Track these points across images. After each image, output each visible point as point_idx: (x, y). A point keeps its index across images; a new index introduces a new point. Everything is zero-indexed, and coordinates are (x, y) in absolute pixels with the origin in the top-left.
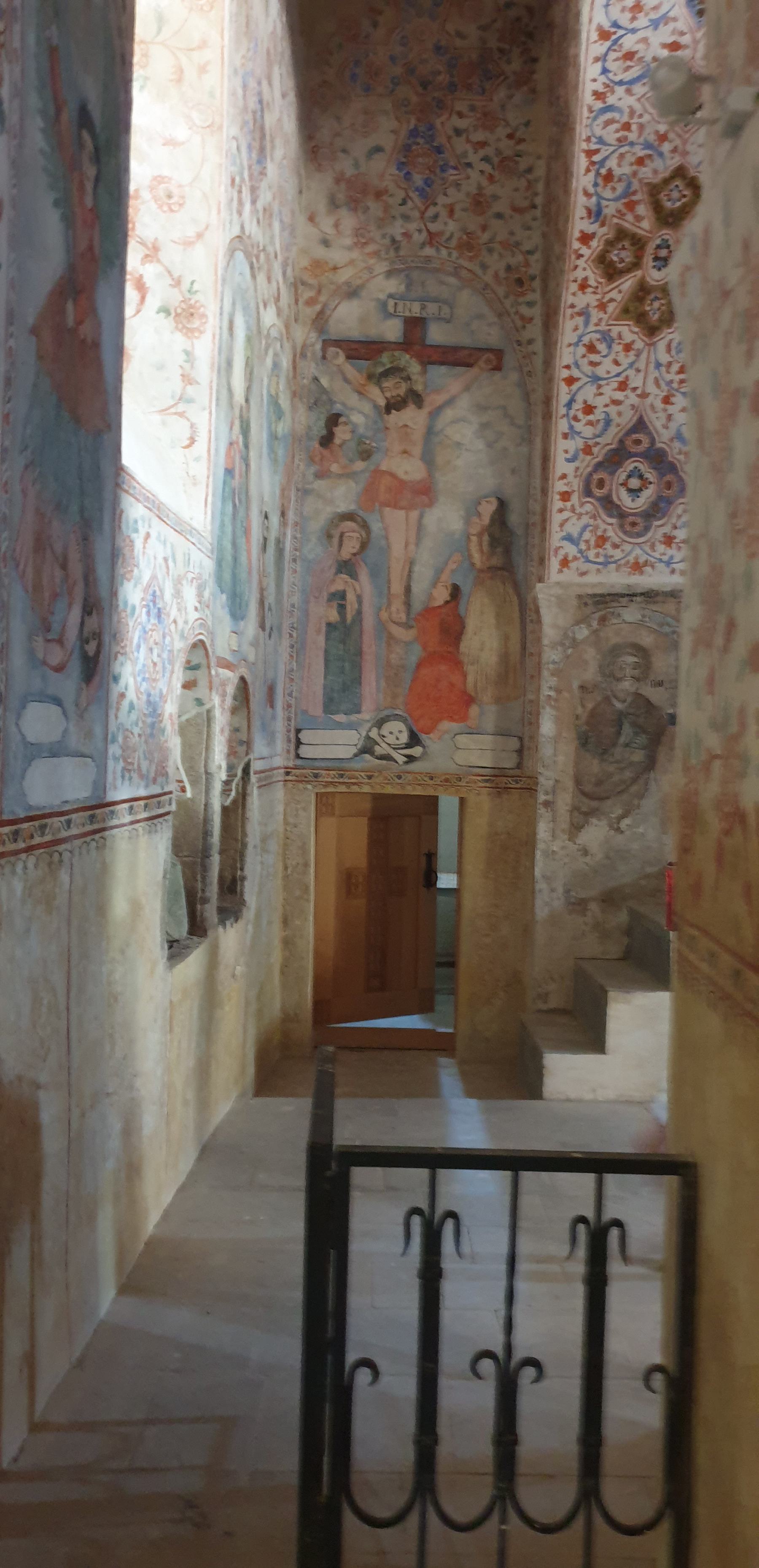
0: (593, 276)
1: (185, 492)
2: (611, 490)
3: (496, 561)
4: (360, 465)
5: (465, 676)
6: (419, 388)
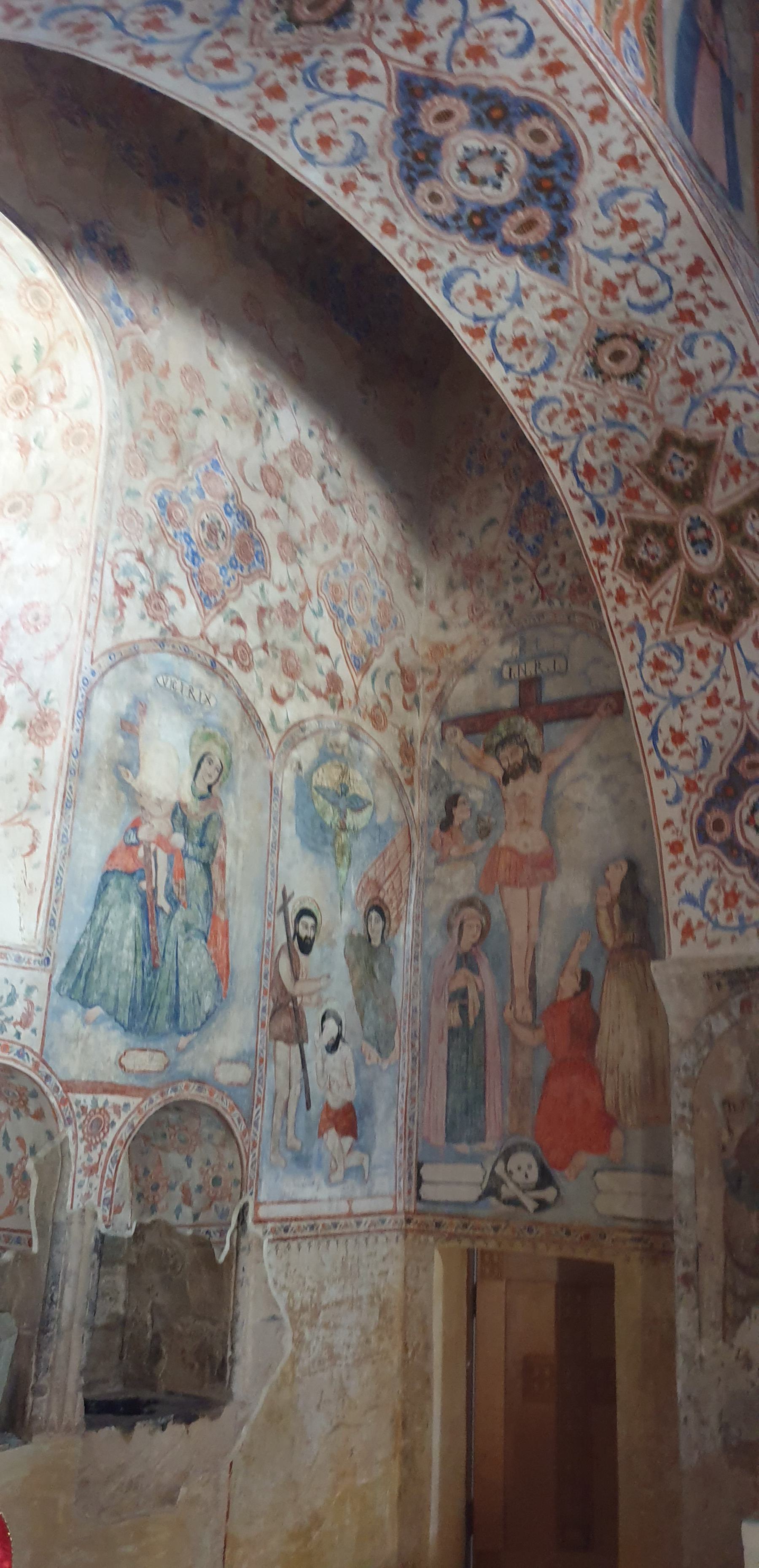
1: (19, 901)
2: (733, 831)
3: (629, 937)
4: (479, 844)
5: (602, 1089)
6: (536, 750)
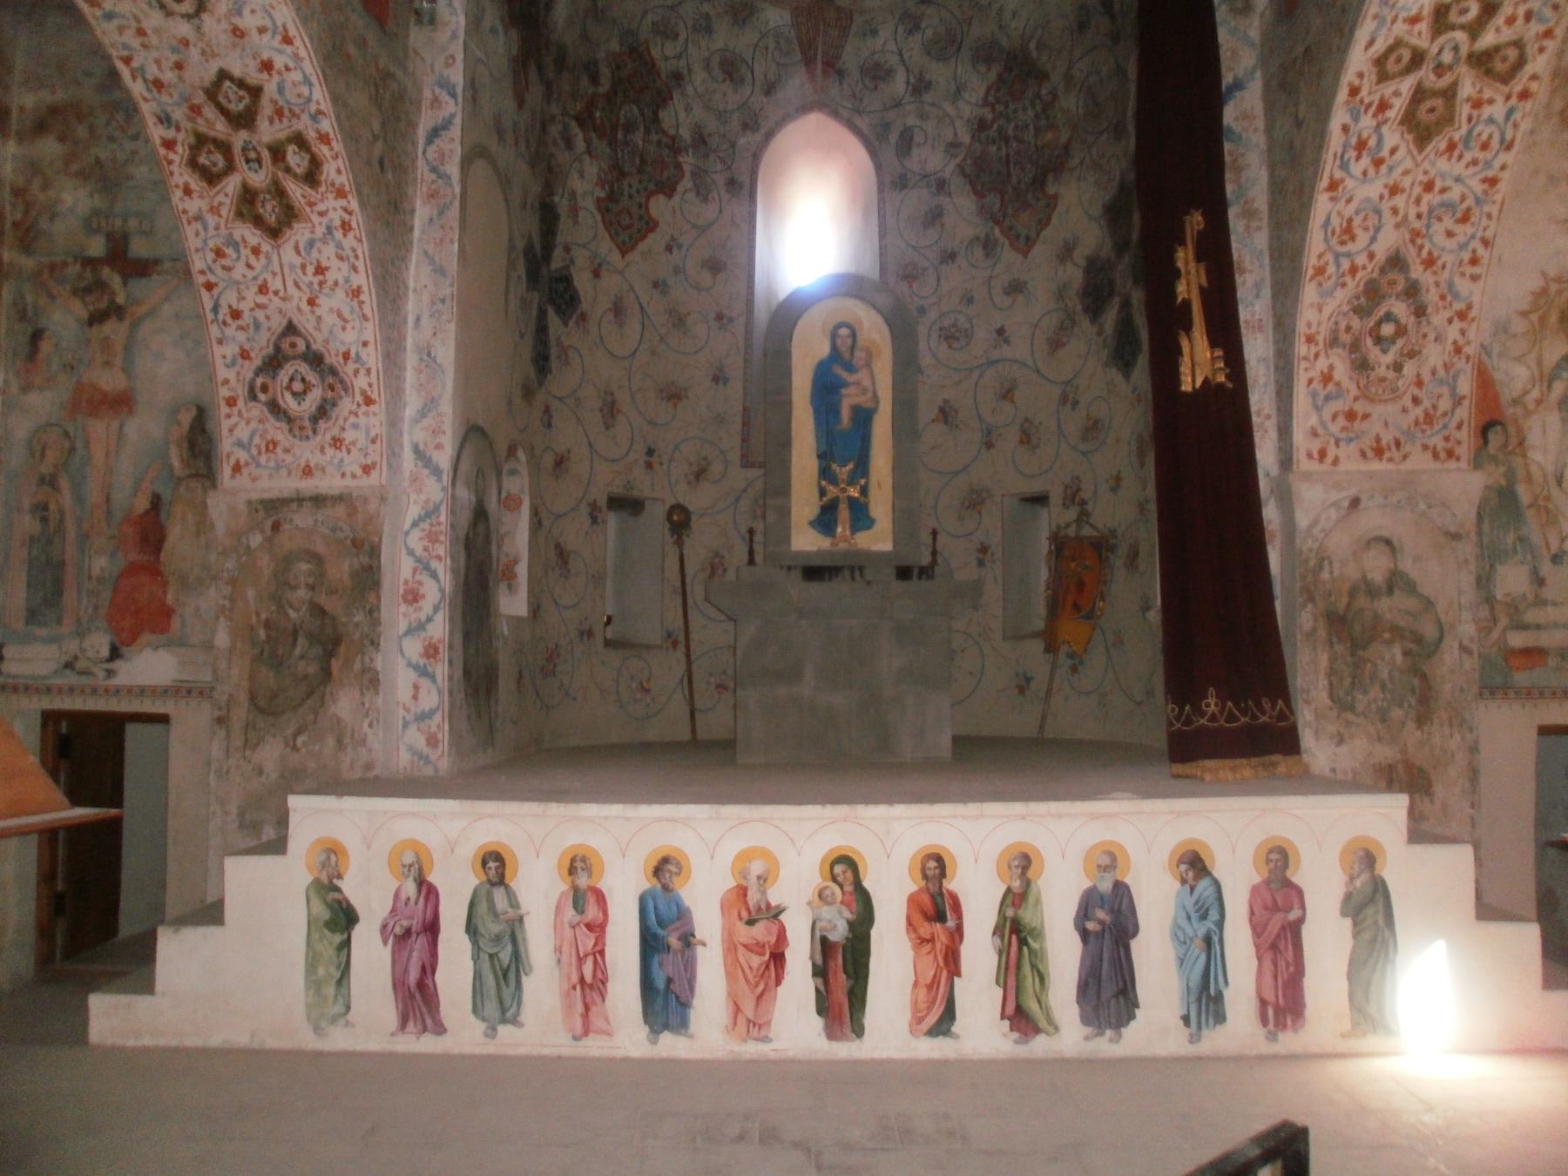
0: (195, 183)
6: (120, 300)
